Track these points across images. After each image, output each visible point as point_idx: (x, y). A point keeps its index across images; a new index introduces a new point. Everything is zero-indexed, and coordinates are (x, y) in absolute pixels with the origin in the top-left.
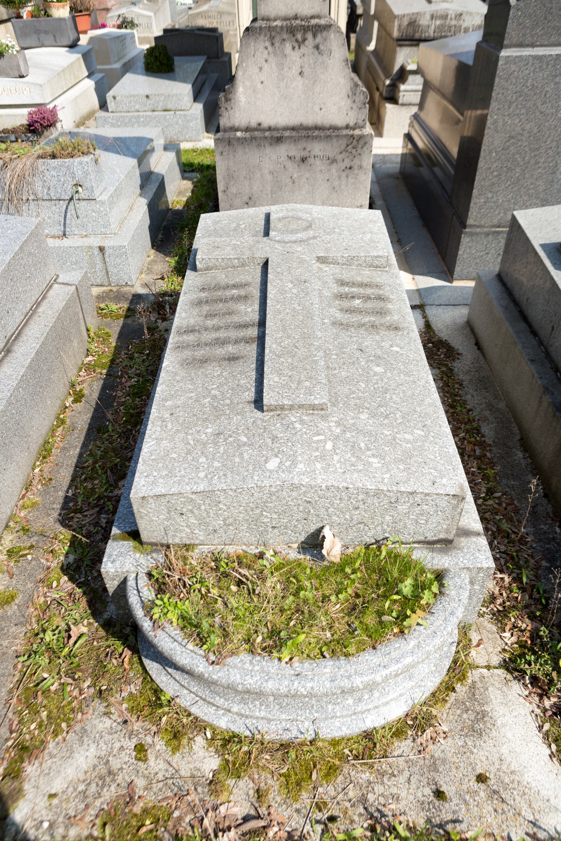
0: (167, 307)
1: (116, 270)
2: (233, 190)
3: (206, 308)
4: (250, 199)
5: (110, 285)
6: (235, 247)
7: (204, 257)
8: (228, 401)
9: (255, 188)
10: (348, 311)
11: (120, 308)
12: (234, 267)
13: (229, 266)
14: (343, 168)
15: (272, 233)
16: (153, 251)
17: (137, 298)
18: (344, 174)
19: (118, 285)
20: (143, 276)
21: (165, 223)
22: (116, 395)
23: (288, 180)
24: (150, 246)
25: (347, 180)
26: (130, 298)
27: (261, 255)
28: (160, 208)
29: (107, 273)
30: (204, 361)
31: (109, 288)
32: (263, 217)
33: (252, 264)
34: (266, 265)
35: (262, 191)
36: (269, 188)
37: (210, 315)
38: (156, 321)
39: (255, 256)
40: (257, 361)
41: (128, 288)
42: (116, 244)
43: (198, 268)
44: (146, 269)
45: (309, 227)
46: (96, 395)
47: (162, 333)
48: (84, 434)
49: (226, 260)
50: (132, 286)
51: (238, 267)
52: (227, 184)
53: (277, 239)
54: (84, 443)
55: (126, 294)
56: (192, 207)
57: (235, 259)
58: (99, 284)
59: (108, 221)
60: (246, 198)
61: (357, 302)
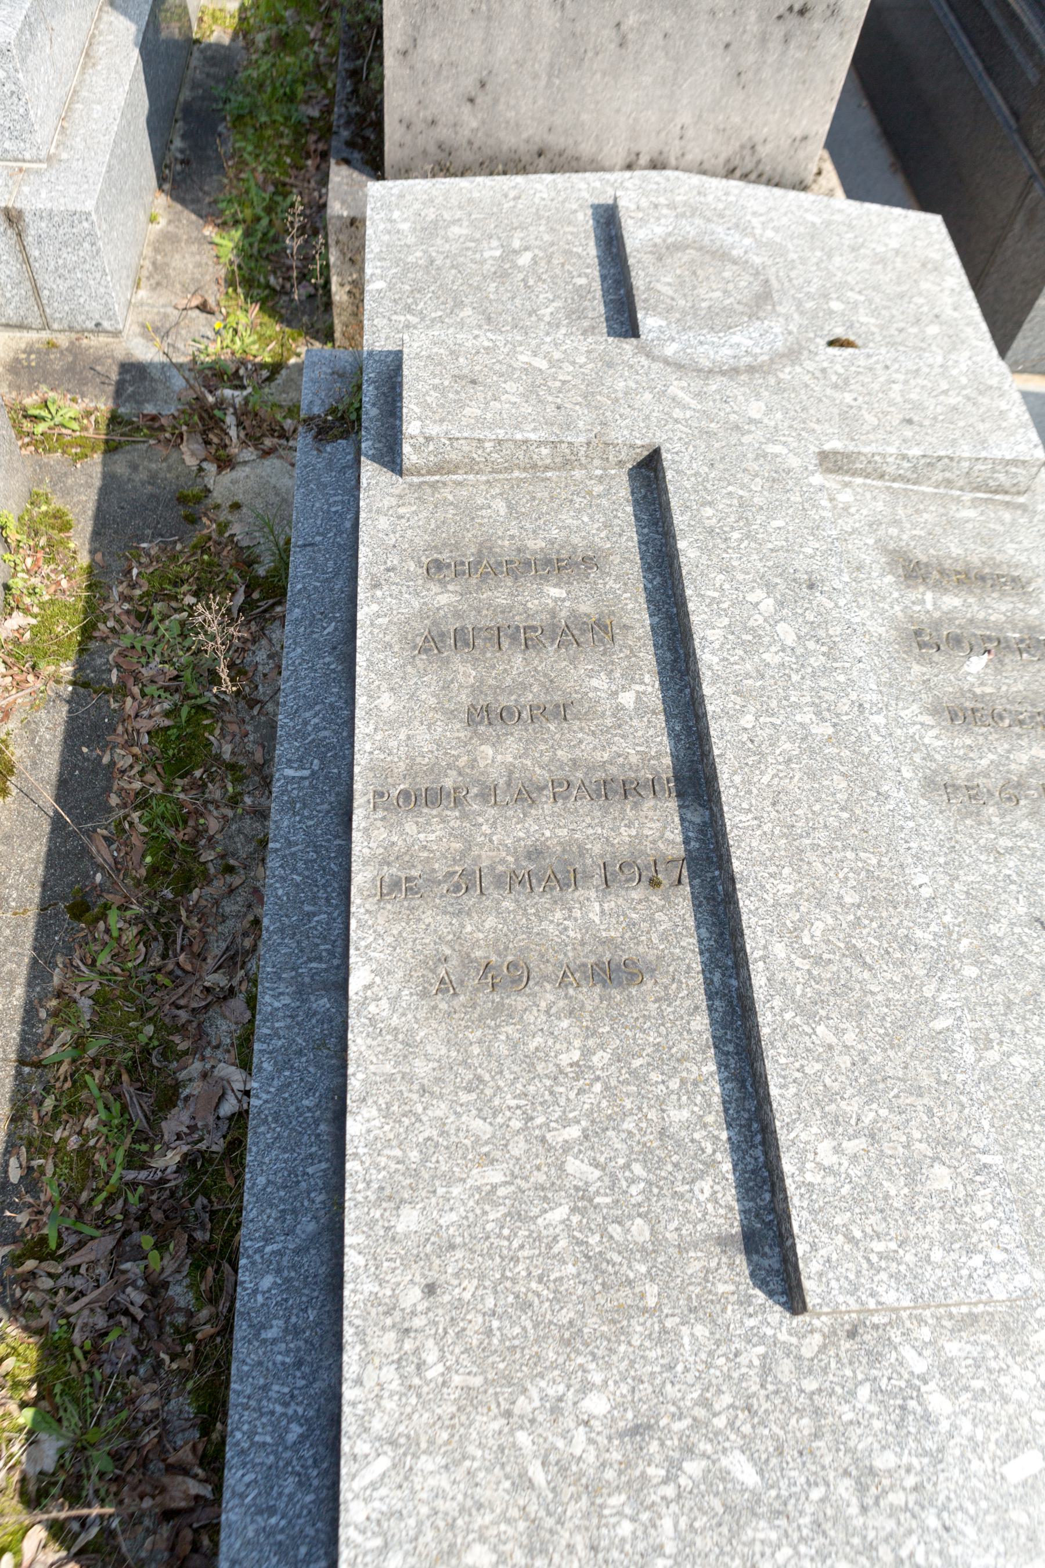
0: (230, 420)
1: (63, 286)
2: (432, 50)
3: (465, 672)
4: (483, 85)
5: (47, 326)
6: (535, 386)
7: (434, 430)
8: (640, 1231)
9: (501, 52)
10: (962, 714)
11: (88, 414)
12: (534, 466)
13: (518, 466)
14: (782, 9)
15: (648, 322)
16: (162, 200)
17: (134, 376)
18: (778, 31)
19: (71, 329)
20: (143, 293)
21: (186, 94)
22: (112, 763)
23: (608, 33)
24: (154, 183)
25: (783, 53)
26: (114, 377)
27: (633, 438)
28: (163, 35)
29: (36, 290)
30: (506, 976)
31: (45, 335)
32: (585, 221)
33: (597, 462)
34: (649, 472)
35: (520, 64)
36: (545, 56)
37: (486, 716)
38: (201, 469)
39: (612, 435)
40: (710, 996)
41: (103, 339)
42: (61, 204)
43: (406, 464)
44: (147, 264)
45: (762, 300)
46: (51, 765)
47: (224, 516)
48: (31, 924)
49: (508, 449)
50: (116, 334)
51: (547, 468)
52: (415, 27)
53: (670, 350)
54: (34, 962)
55: (98, 360)
56: (260, 38)
57: (541, 443)
58: (14, 321)
59: (25, 116)
60: (468, 83)
61: (977, 663)
